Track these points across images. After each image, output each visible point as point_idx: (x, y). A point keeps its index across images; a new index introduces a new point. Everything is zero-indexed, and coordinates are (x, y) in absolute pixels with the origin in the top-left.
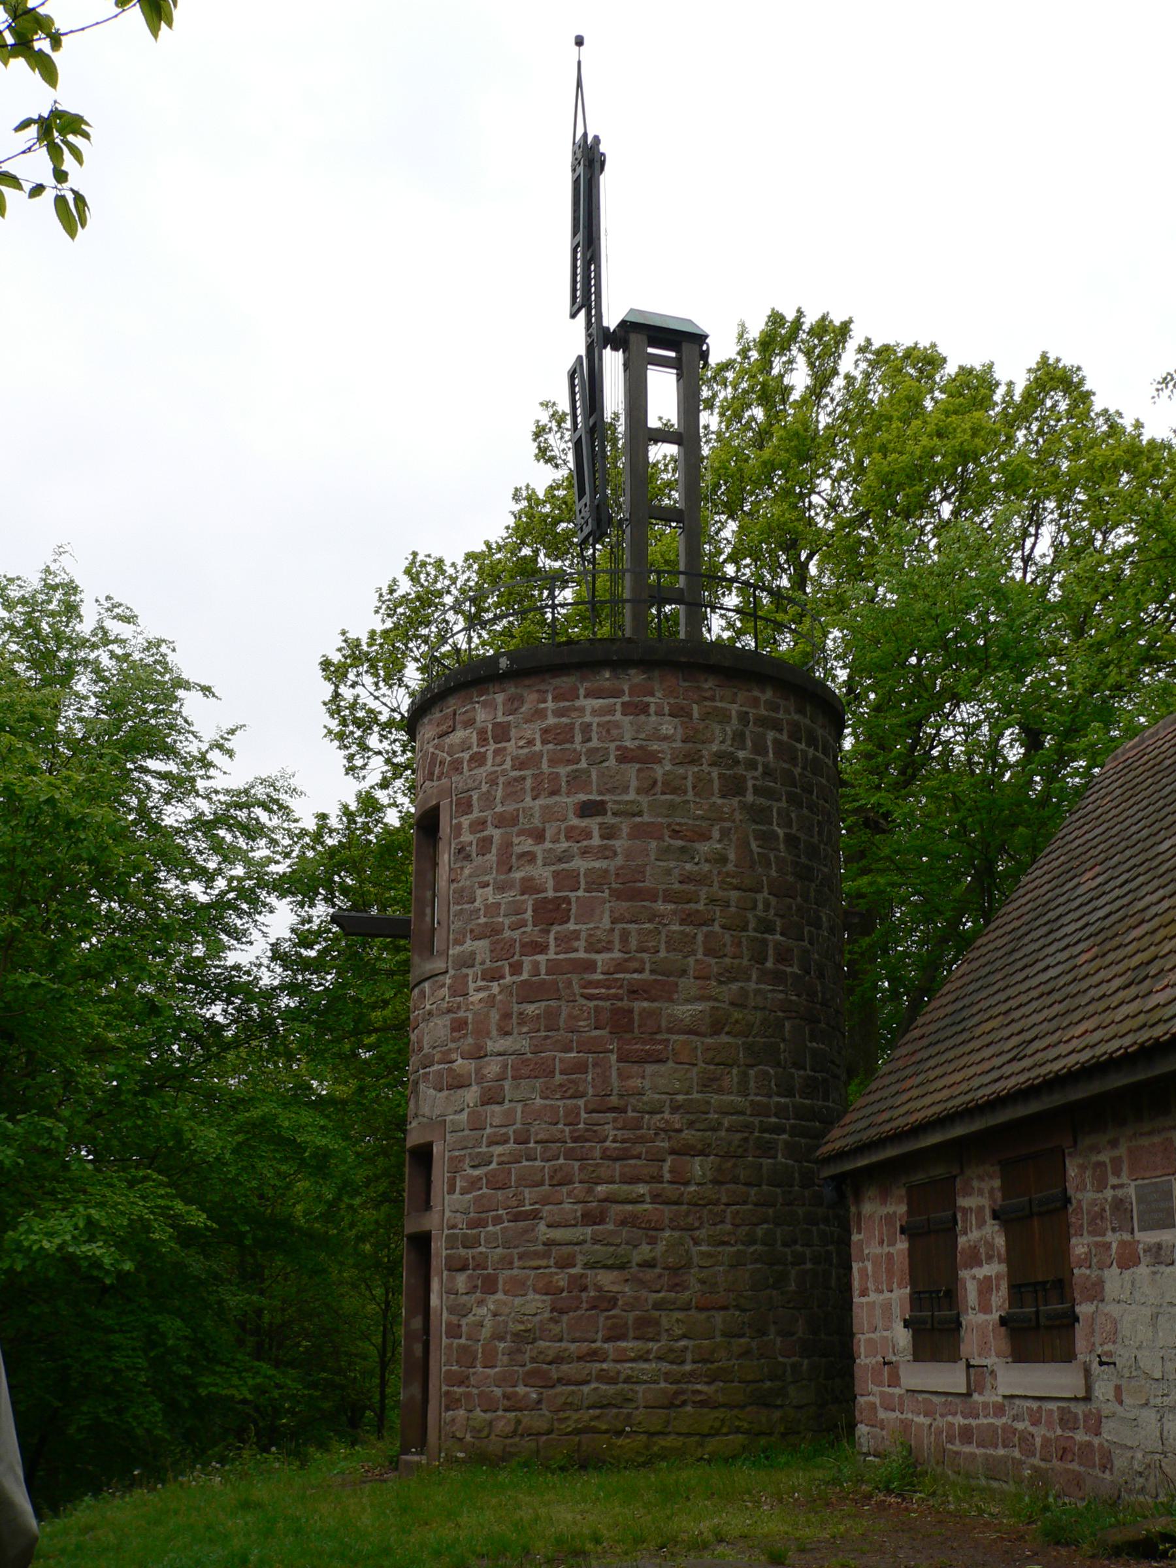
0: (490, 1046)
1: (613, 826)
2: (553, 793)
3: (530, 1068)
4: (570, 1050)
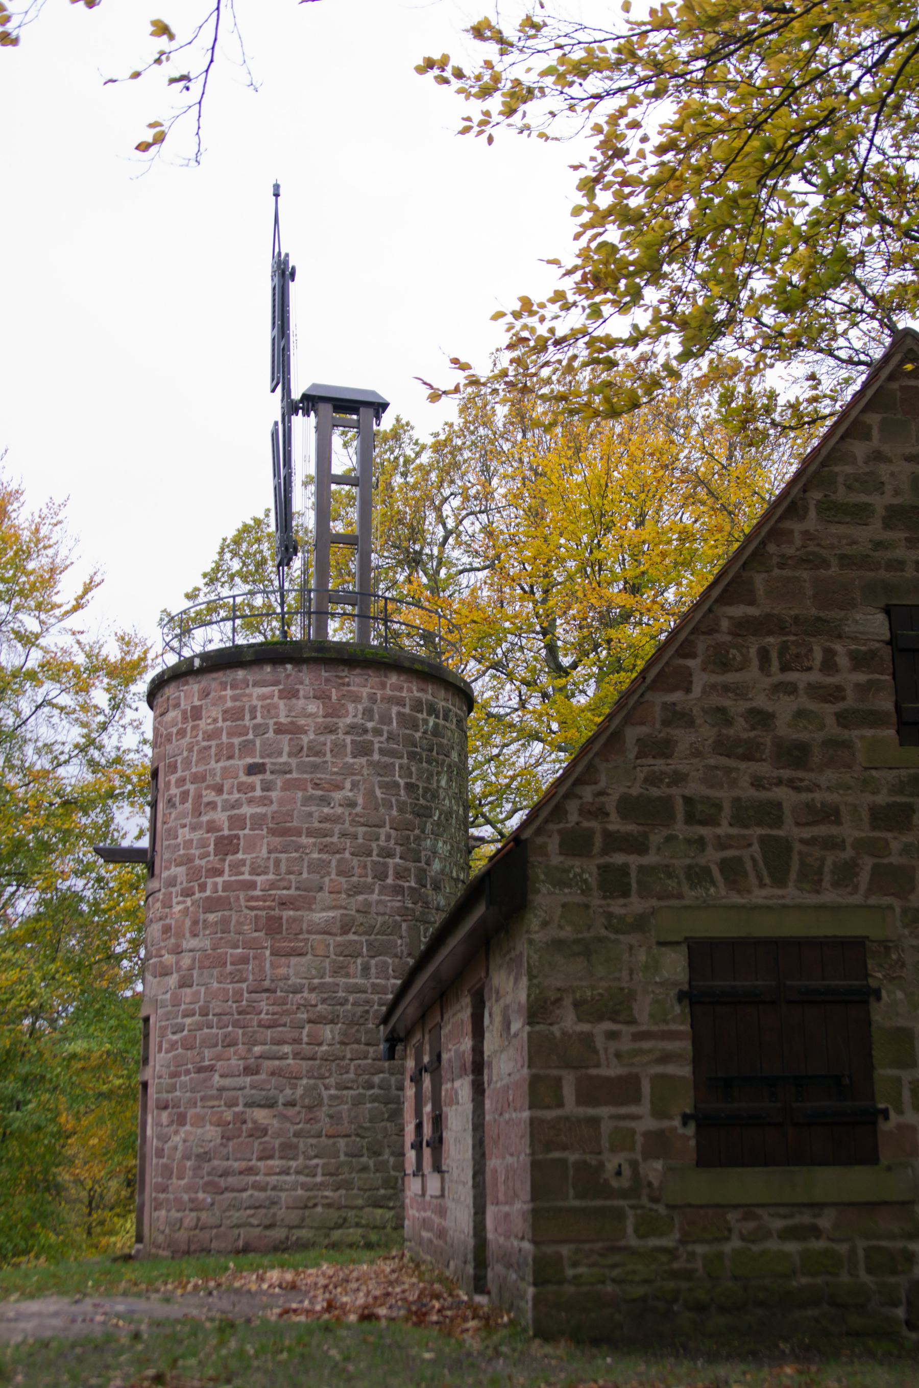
0: (185, 945)
1: (271, 781)
2: (230, 757)
3: (211, 961)
4: (237, 947)
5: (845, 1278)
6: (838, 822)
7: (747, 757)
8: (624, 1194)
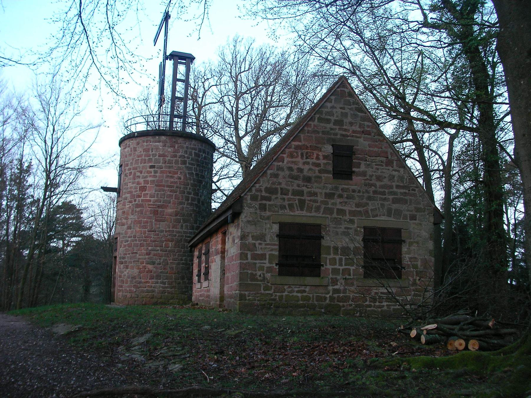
2: (145, 163)
5: (310, 302)
6: (317, 196)
7: (296, 179)
8: (261, 281)
